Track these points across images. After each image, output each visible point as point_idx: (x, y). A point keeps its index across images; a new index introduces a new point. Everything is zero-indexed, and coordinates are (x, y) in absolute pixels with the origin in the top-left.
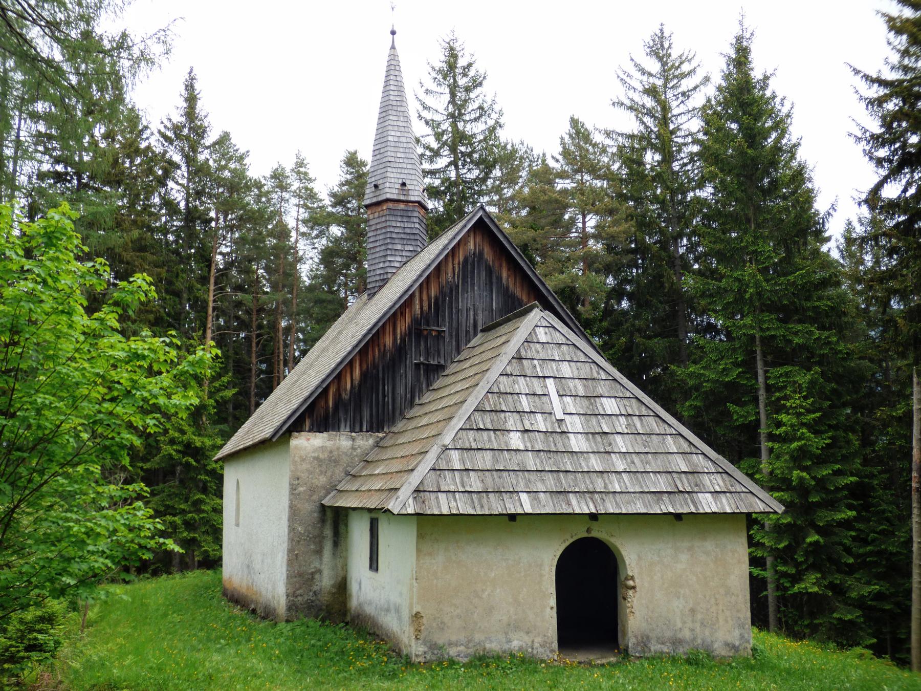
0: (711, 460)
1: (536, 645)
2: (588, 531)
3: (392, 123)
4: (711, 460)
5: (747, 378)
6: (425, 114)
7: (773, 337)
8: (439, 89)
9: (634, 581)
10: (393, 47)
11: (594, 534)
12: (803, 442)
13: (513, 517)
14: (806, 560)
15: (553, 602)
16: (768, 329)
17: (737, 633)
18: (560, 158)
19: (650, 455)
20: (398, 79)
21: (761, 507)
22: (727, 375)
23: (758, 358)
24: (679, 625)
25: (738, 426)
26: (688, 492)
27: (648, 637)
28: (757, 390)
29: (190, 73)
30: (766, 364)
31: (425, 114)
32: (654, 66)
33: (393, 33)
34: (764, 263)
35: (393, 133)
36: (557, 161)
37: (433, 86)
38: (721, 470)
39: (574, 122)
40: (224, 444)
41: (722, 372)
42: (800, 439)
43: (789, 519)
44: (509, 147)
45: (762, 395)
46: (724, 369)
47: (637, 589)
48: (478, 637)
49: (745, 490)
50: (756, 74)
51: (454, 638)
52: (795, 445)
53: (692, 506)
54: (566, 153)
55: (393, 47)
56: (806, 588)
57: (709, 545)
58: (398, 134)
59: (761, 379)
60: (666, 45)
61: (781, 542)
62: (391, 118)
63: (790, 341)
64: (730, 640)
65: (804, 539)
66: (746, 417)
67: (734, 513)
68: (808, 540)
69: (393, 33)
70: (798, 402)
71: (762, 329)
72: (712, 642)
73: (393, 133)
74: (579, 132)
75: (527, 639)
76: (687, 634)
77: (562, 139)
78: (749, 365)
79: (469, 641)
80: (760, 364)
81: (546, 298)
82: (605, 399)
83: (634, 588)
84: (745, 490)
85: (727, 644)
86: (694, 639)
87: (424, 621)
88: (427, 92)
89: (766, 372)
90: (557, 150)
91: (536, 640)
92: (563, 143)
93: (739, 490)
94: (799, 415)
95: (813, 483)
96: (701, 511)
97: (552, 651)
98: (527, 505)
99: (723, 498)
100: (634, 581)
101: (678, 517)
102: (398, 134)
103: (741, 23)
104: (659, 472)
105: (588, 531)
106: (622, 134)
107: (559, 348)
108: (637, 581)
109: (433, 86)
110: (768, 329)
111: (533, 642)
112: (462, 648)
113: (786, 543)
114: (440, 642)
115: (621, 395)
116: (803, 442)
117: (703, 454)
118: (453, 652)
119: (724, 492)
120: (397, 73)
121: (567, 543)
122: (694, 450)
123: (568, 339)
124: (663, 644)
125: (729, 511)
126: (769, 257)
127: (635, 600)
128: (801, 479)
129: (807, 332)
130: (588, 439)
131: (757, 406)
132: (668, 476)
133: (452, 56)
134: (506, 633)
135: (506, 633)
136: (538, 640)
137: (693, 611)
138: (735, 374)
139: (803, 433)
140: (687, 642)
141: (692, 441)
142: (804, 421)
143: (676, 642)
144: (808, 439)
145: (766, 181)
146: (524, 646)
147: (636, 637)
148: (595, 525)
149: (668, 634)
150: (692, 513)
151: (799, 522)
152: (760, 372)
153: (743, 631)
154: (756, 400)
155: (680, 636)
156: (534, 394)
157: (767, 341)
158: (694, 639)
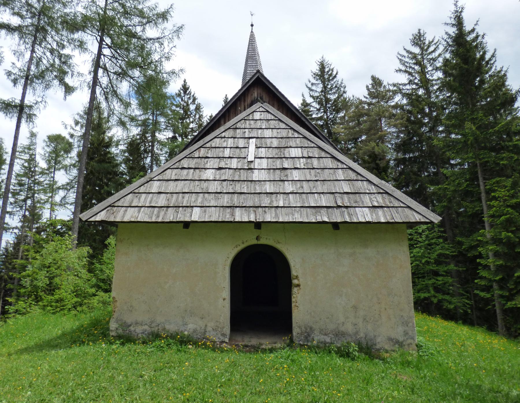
0: (374, 185)
1: (209, 329)
2: (258, 238)
3: (250, 65)
4: (374, 185)
5: (473, 187)
6: (312, 93)
7: (487, 162)
8: (317, 82)
9: (298, 280)
10: (252, 32)
11: (263, 241)
12: (508, 216)
13: (187, 225)
14: (516, 288)
15: (226, 294)
16: (483, 158)
17: (401, 329)
18: (368, 96)
19: (319, 182)
20: (253, 45)
21: (418, 218)
22: (460, 187)
23: (480, 176)
24: (342, 319)
25: (471, 215)
26: (347, 207)
27: (311, 328)
28: (480, 193)
29: (226, 97)
30: (484, 179)
31: (312, 93)
32: (416, 50)
33: (252, 25)
34: (478, 123)
35: (250, 69)
36: (367, 98)
37: (314, 81)
38: (382, 191)
39: (374, 78)
40: (97, 204)
41: (457, 185)
42: (506, 215)
43: (501, 262)
44: (347, 99)
45: (483, 196)
46: (459, 184)
47: (301, 287)
48: (159, 319)
49: (402, 205)
50: (468, 27)
51: (140, 319)
52: (503, 218)
53: (347, 217)
54: (371, 94)
55: (252, 32)
56: (515, 304)
57: (370, 251)
58: (252, 69)
59: (482, 187)
60: (422, 39)
61: (497, 276)
62: (249, 62)
63: (498, 164)
64: (393, 336)
65: (513, 275)
66: (474, 208)
67: (388, 223)
68: (516, 275)
69: (252, 25)
70: (503, 193)
71: (480, 159)
72: (375, 336)
73: (250, 69)
74: (376, 82)
75: (201, 324)
76: (349, 328)
77: (367, 87)
78: (474, 178)
79: (152, 322)
80: (481, 179)
81: (300, 119)
82: (293, 149)
83: (298, 286)
84: (402, 205)
85: (390, 339)
86: (357, 333)
87: (118, 304)
88: (312, 84)
89: (485, 183)
90: (366, 93)
91: (209, 325)
92: (368, 89)
93: (396, 205)
94: (505, 200)
95: (517, 240)
96: (355, 220)
97: (224, 335)
98: (196, 215)
99: (380, 212)
100: (298, 280)
101: (336, 225)
102: (252, 69)
103: (456, 5)
104: (323, 193)
105: (258, 238)
106: (402, 84)
107: (268, 122)
108: (301, 280)
109: (314, 81)
110: (483, 158)
111: (206, 326)
112: (146, 327)
113: (501, 277)
114: (129, 321)
115: (307, 146)
116: (508, 216)
117: (409, 207)
118: (139, 330)
119: (382, 207)
120: (253, 42)
121: (239, 248)
122: (360, 178)
123: (276, 117)
124: (325, 335)
125: (383, 220)
126: (482, 120)
127: (299, 296)
128: (509, 238)
129: (509, 157)
130: (269, 173)
131: (481, 202)
132: (331, 196)
133: (322, 66)
134: (183, 318)
135: (183, 318)
136: (211, 325)
137: (355, 308)
138: (465, 185)
139: (508, 211)
140: (350, 335)
141: (359, 171)
142: (508, 204)
143: (339, 334)
144: (511, 214)
145: (489, 100)
146: (198, 329)
147: (299, 327)
148: (262, 232)
149: (331, 327)
150: (346, 222)
151: (509, 264)
152: (481, 184)
153: (407, 328)
154: (480, 200)
155: (342, 329)
156: (237, 147)
157: (484, 165)
158: (357, 333)
